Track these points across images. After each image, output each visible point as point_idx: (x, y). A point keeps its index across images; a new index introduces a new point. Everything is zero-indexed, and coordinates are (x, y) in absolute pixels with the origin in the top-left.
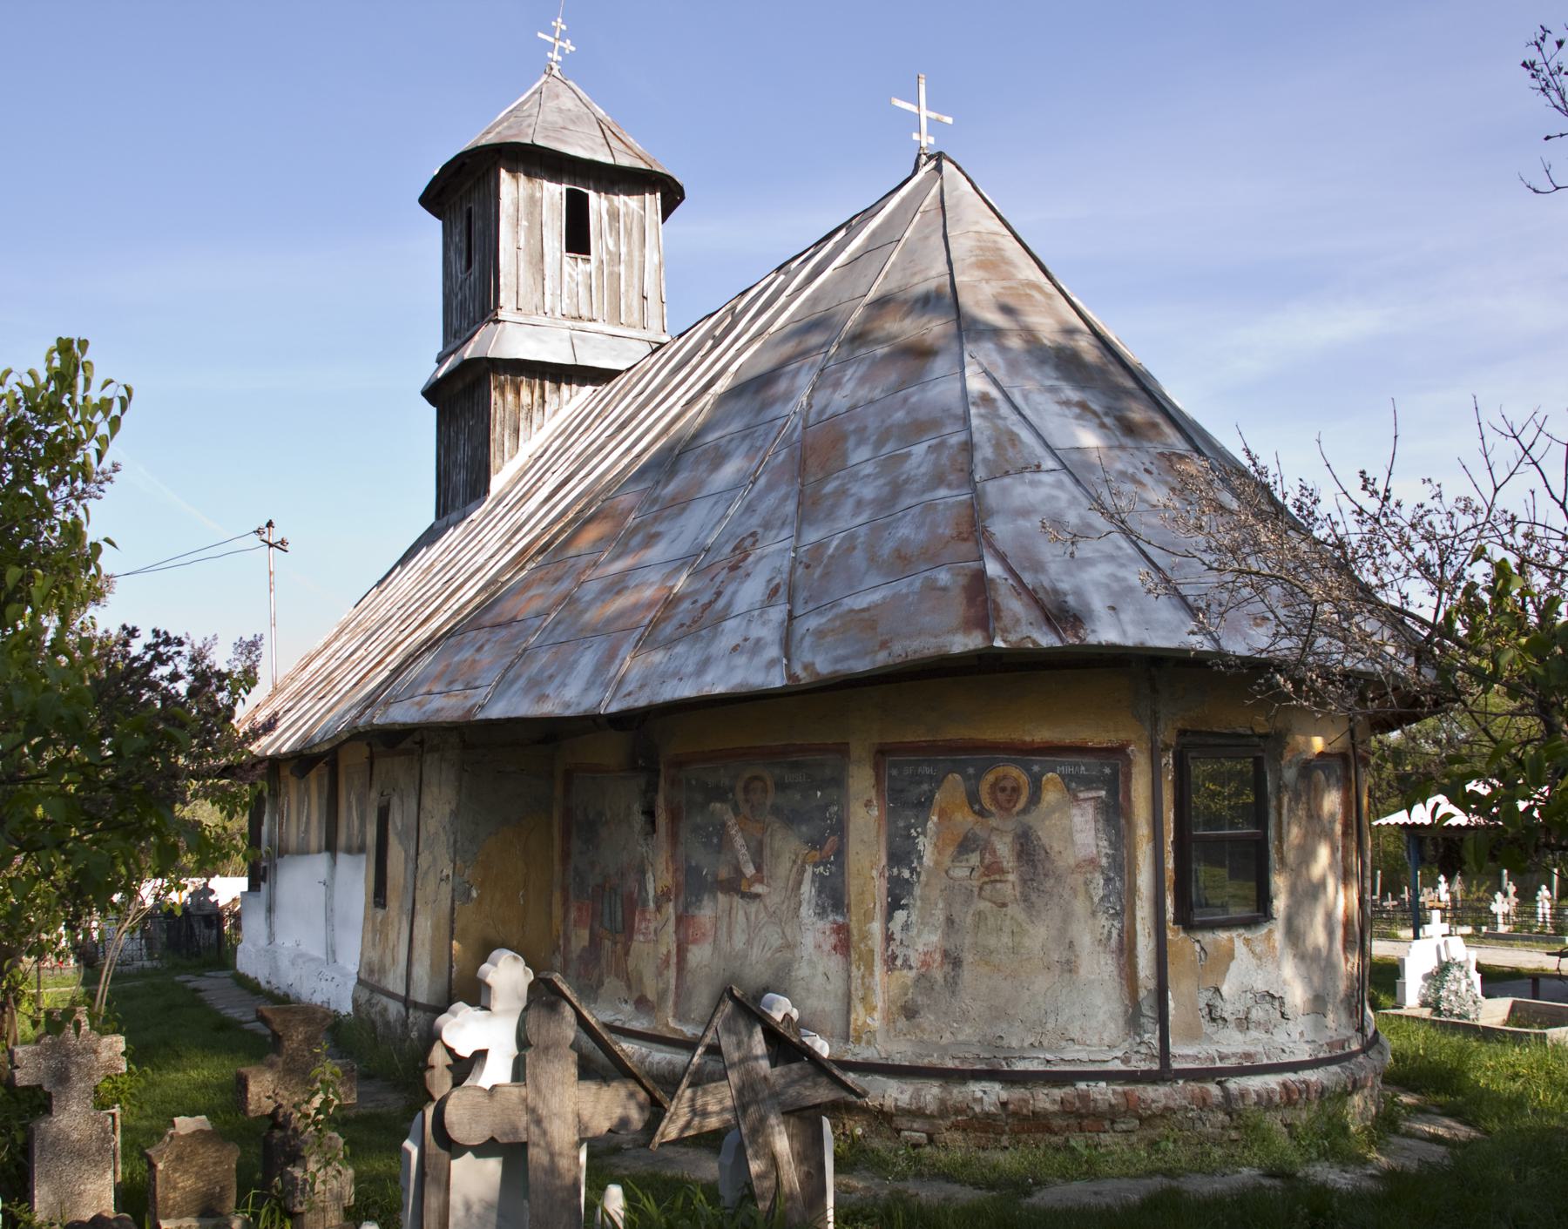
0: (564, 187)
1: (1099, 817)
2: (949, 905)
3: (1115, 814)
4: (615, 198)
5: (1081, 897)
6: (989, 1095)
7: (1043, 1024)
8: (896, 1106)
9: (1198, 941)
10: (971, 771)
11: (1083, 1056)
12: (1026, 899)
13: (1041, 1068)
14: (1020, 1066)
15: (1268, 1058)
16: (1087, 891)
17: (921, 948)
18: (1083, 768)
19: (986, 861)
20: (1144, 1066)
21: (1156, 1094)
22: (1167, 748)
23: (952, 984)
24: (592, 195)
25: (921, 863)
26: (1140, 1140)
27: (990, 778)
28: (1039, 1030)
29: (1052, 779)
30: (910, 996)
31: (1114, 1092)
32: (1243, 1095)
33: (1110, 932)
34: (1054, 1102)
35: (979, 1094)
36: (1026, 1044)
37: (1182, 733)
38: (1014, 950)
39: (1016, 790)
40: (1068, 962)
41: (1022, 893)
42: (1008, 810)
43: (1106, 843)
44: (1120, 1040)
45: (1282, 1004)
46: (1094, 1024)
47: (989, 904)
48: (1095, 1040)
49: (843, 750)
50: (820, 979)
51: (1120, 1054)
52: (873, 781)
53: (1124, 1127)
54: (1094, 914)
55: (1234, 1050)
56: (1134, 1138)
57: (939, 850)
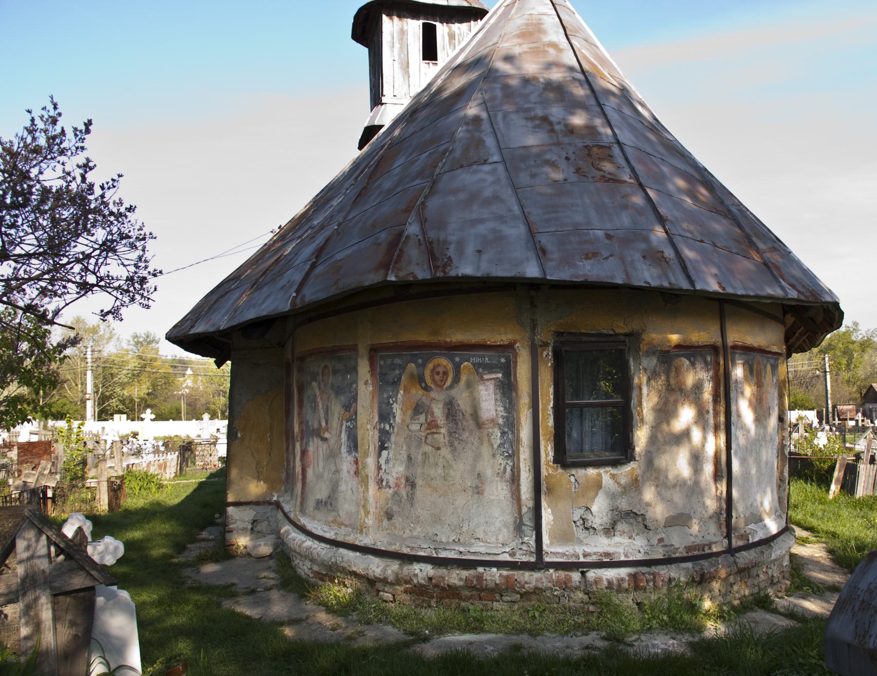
0: (421, 22)
1: (497, 391)
2: (409, 448)
3: (507, 388)
4: (452, 25)
5: (486, 444)
6: (422, 571)
7: (461, 528)
8: (374, 576)
9: (573, 475)
10: (420, 361)
11: (483, 550)
12: (451, 445)
13: (456, 556)
14: (443, 554)
15: (626, 556)
16: (489, 441)
17: (394, 475)
18: (487, 359)
19: (429, 420)
20: (525, 559)
21: (531, 579)
22: (545, 345)
23: (411, 498)
24: (438, 25)
25: (394, 421)
26: (519, 608)
27: (431, 366)
28: (458, 531)
29: (467, 366)
30: (389, 505)
31: (501, 575)
32: (597, 581)
33: (505, 468)
34: (461, 579)
35: (417, 571)
36: (451, 540)
37: (559, 334)
38: (445, 478)
39: (445, 373)
40: (477, 487)
41: (449, 441)
42: (441, 387)
43: (502, 409)
44: (511, 540)
45: (644, 519)
46: (493, 529)
47: (430, 448)
48: (493, 539)
49: (355, 348)
50: (349, 492)
51: (508, 550)
52: (368, 368)
53: (509, 599)
54: (494, 456)
55: (596, 550)
56: (516, 607)
57: (404, 413)
